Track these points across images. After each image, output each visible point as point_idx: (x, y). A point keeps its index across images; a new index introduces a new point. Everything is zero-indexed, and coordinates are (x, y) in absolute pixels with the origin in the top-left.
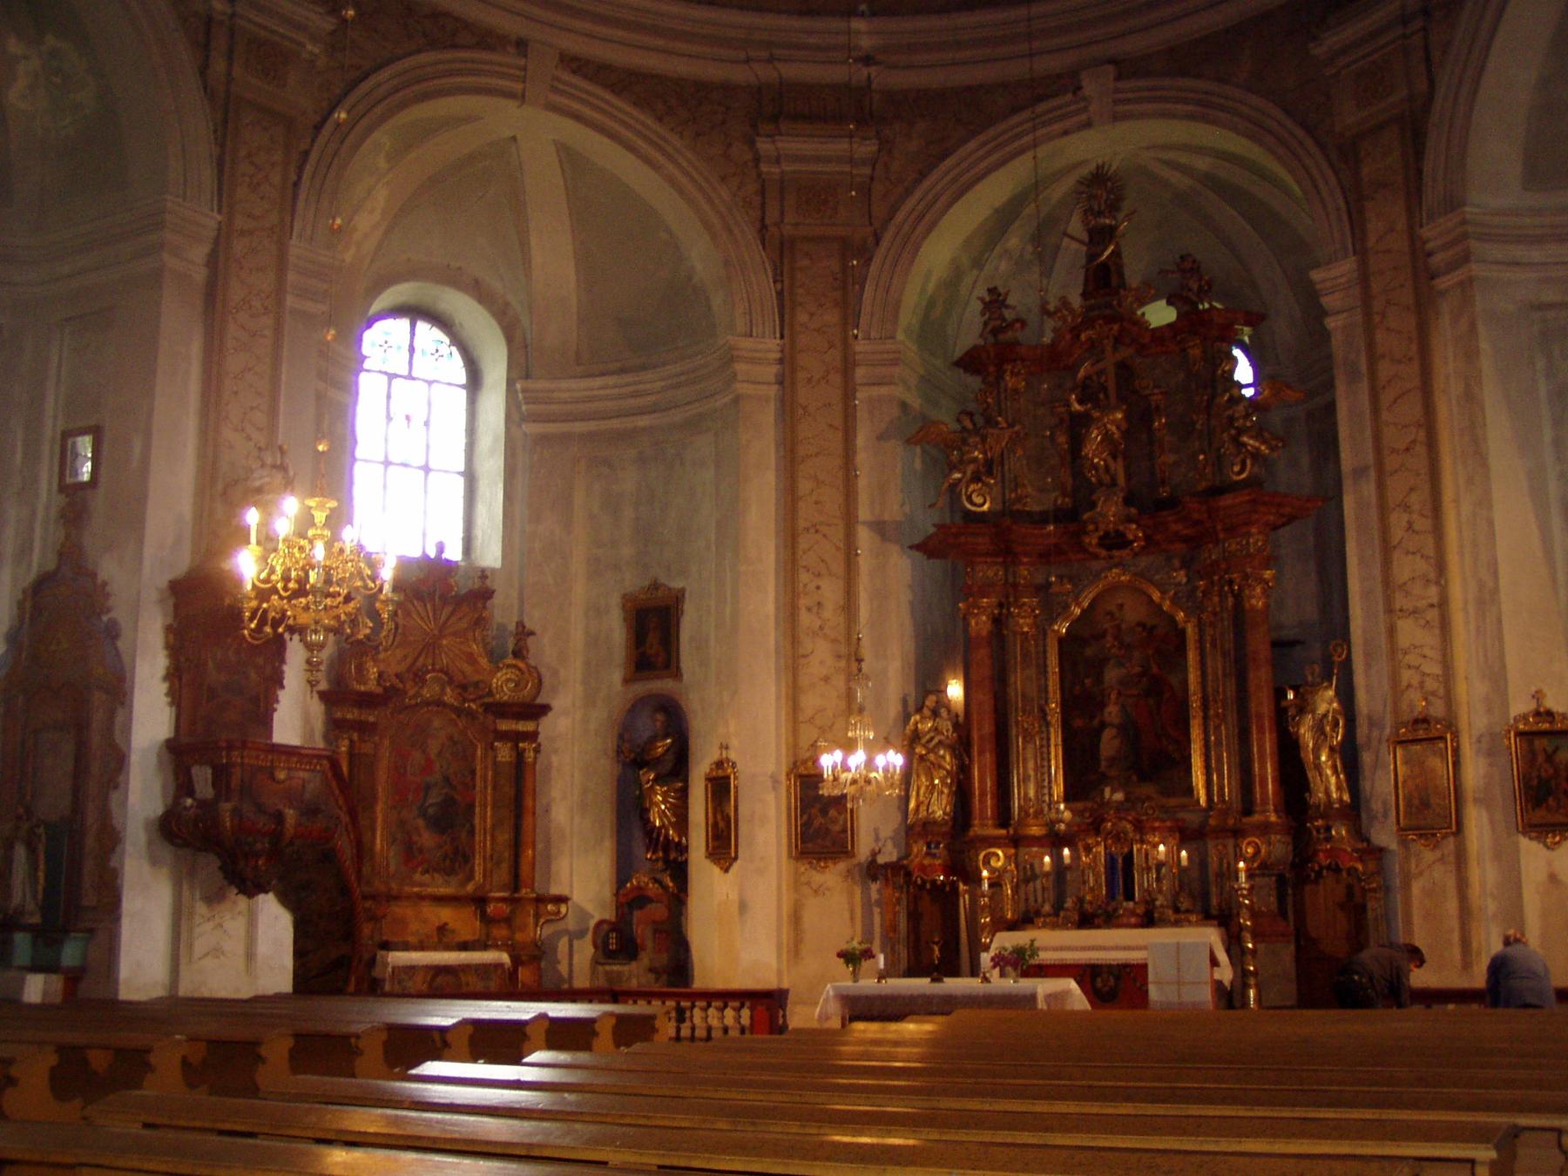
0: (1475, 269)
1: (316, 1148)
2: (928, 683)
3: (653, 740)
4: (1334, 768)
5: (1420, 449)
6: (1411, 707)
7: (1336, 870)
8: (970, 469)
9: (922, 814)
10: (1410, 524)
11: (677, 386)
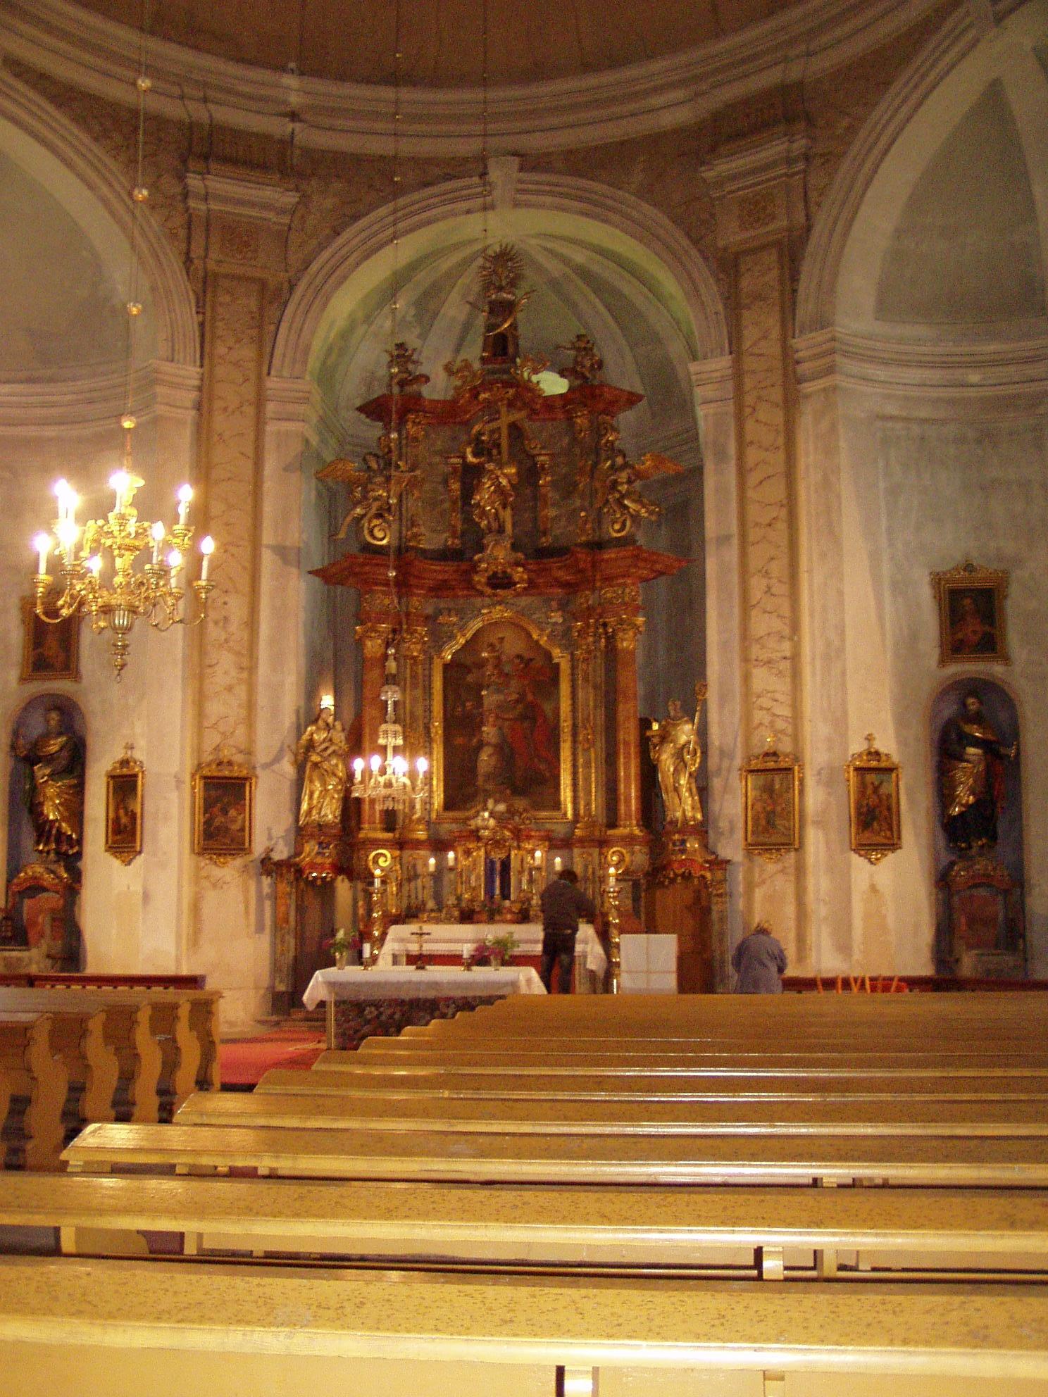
0: (837, 379)
1: (144, 1144)
2: (311, 694)
3: (46, 737)
4: (690, 790)
5: (782, 526)
6: (763, 741)
7: (687, 877)
8: (375, 506)
9: (315, 816)
10: (769, 588)
11: (91, 402)
